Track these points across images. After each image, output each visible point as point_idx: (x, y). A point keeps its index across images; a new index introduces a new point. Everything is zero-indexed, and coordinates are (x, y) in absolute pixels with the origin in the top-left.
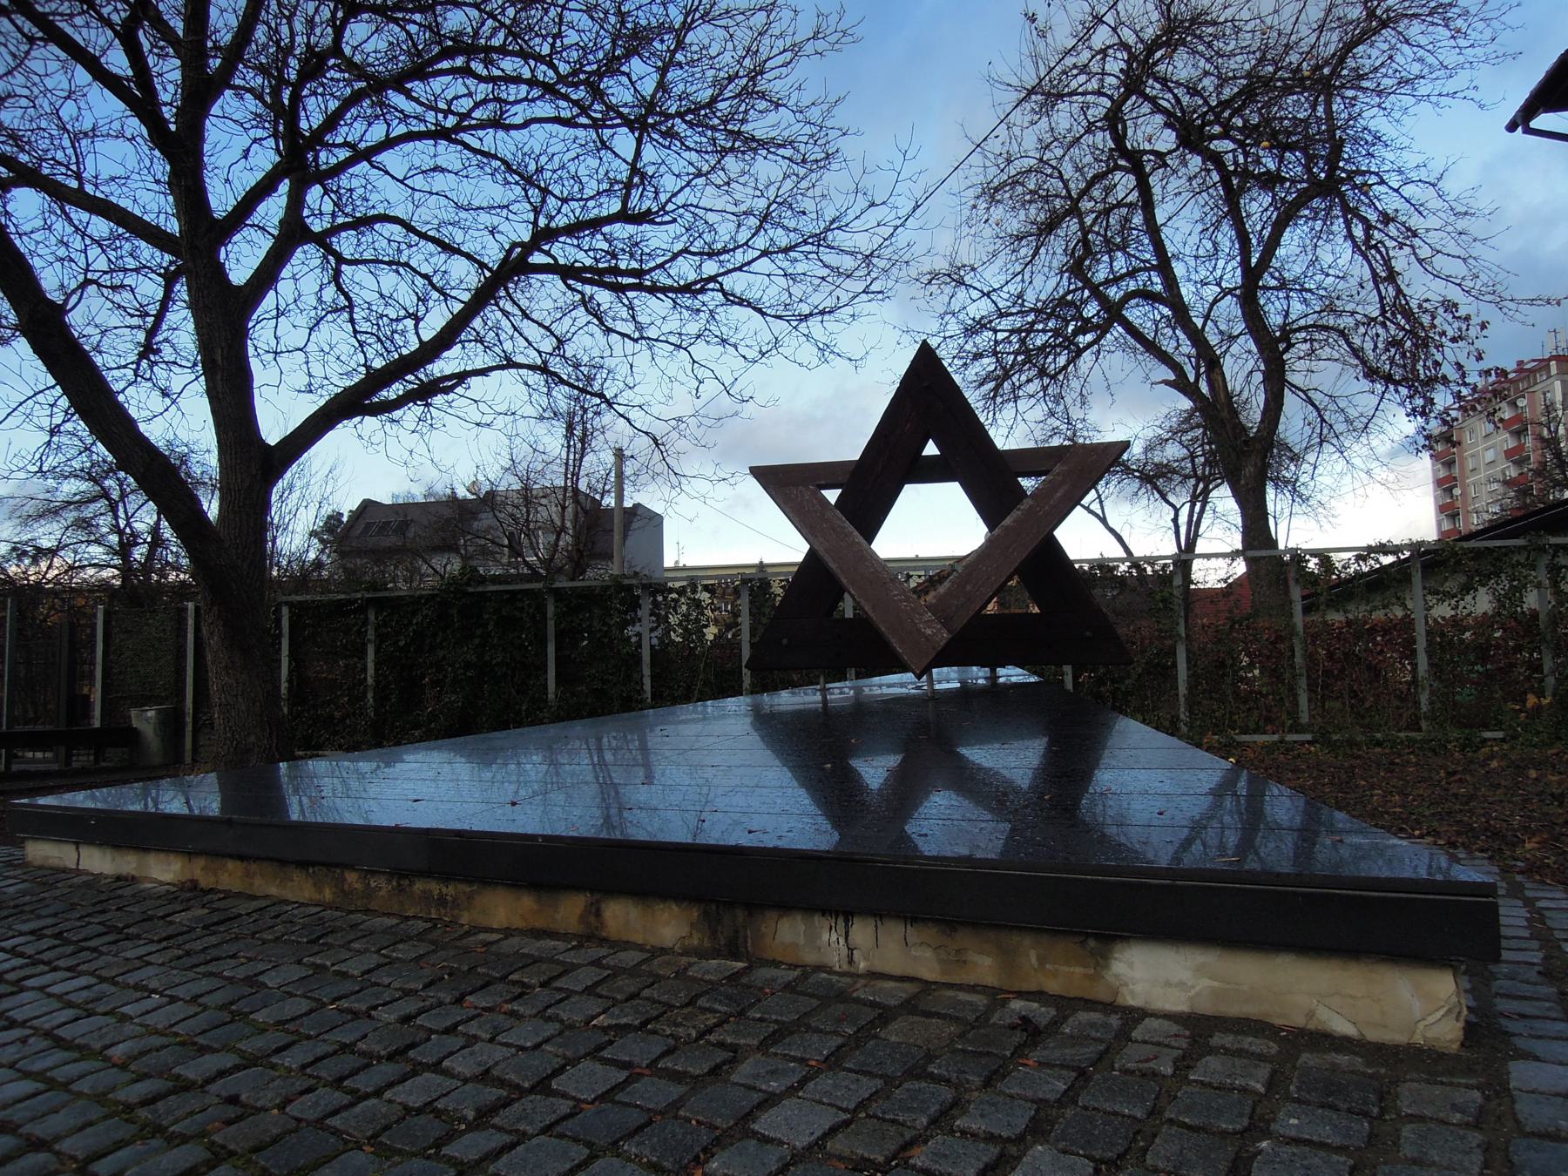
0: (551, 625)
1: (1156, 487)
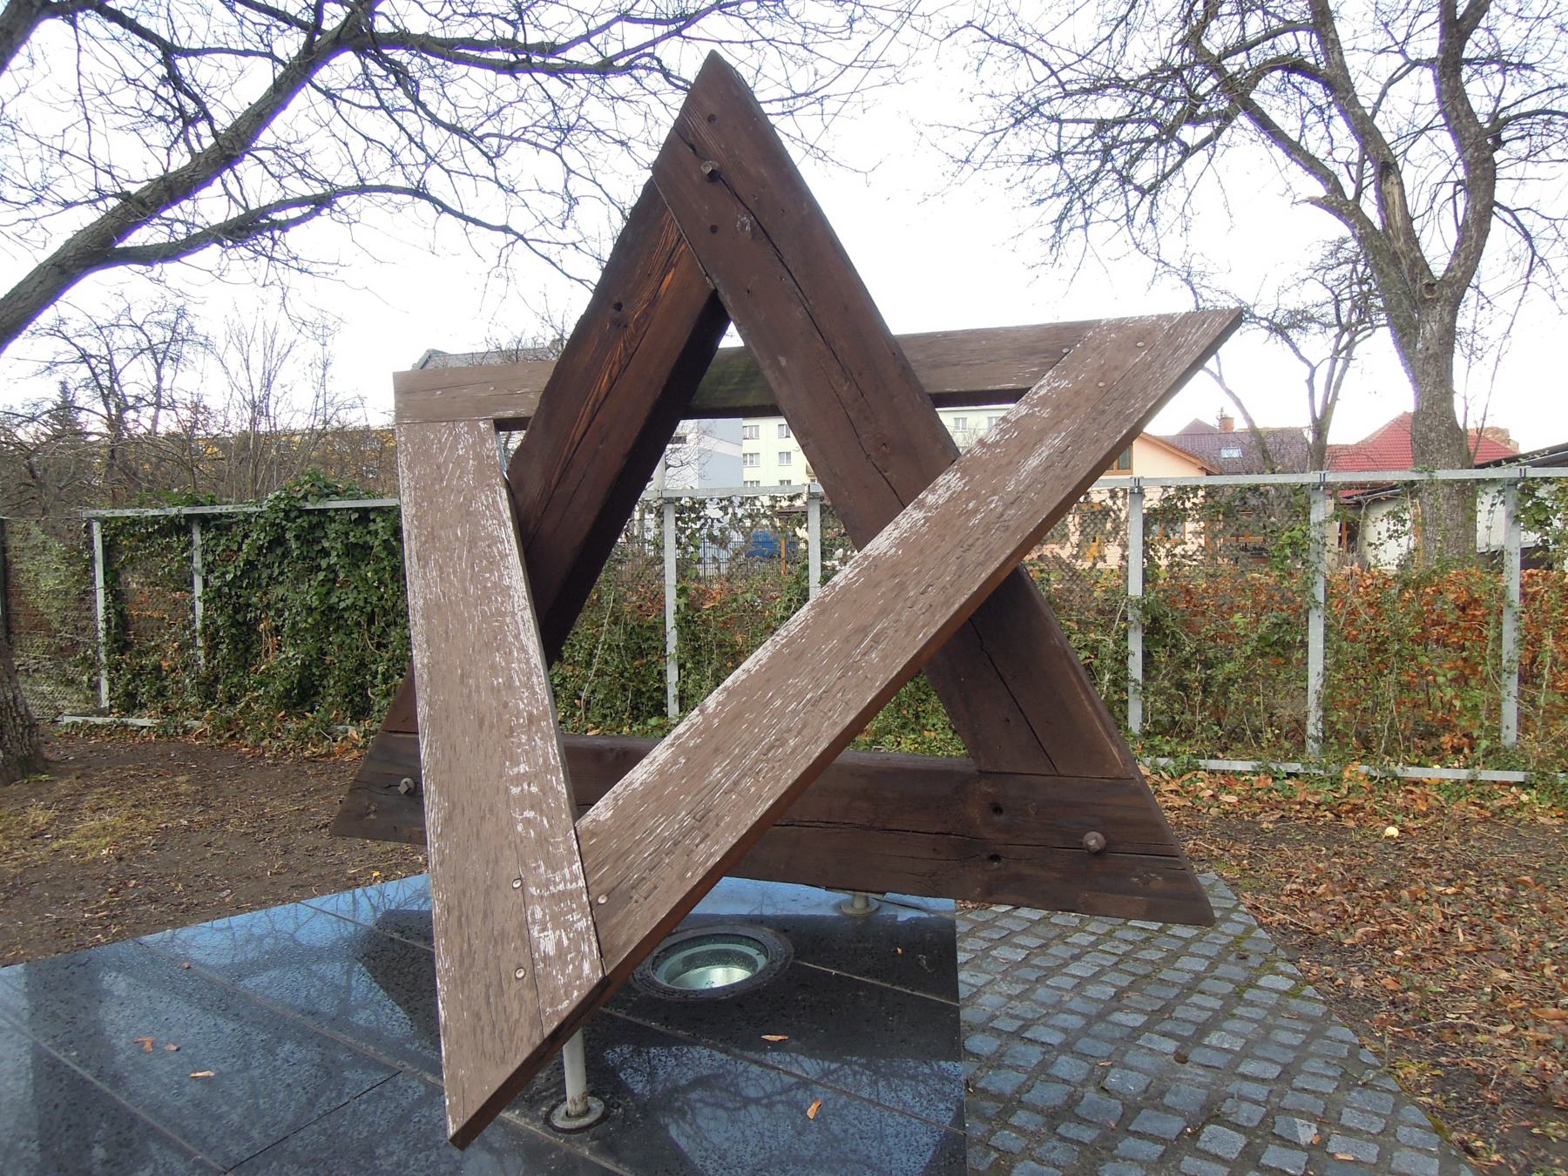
1: (1288, 339)
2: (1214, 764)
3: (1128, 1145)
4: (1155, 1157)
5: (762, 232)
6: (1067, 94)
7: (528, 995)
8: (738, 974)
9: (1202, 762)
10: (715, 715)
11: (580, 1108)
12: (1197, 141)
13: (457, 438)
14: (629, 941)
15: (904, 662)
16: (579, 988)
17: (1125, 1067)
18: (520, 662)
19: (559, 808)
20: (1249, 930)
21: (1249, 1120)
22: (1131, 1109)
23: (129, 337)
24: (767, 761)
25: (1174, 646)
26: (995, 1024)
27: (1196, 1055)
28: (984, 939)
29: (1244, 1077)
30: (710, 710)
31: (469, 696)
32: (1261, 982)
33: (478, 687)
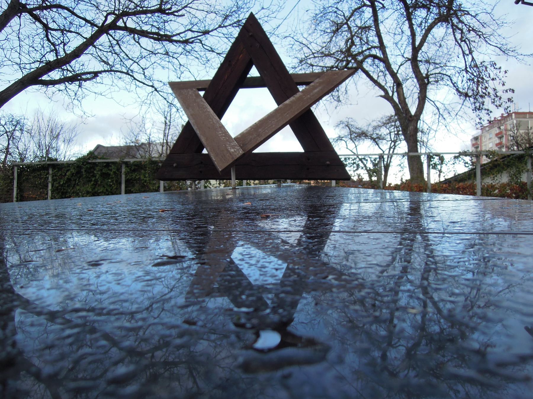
0: (123, 176)
1: (376, 142)
28: (306, 183)
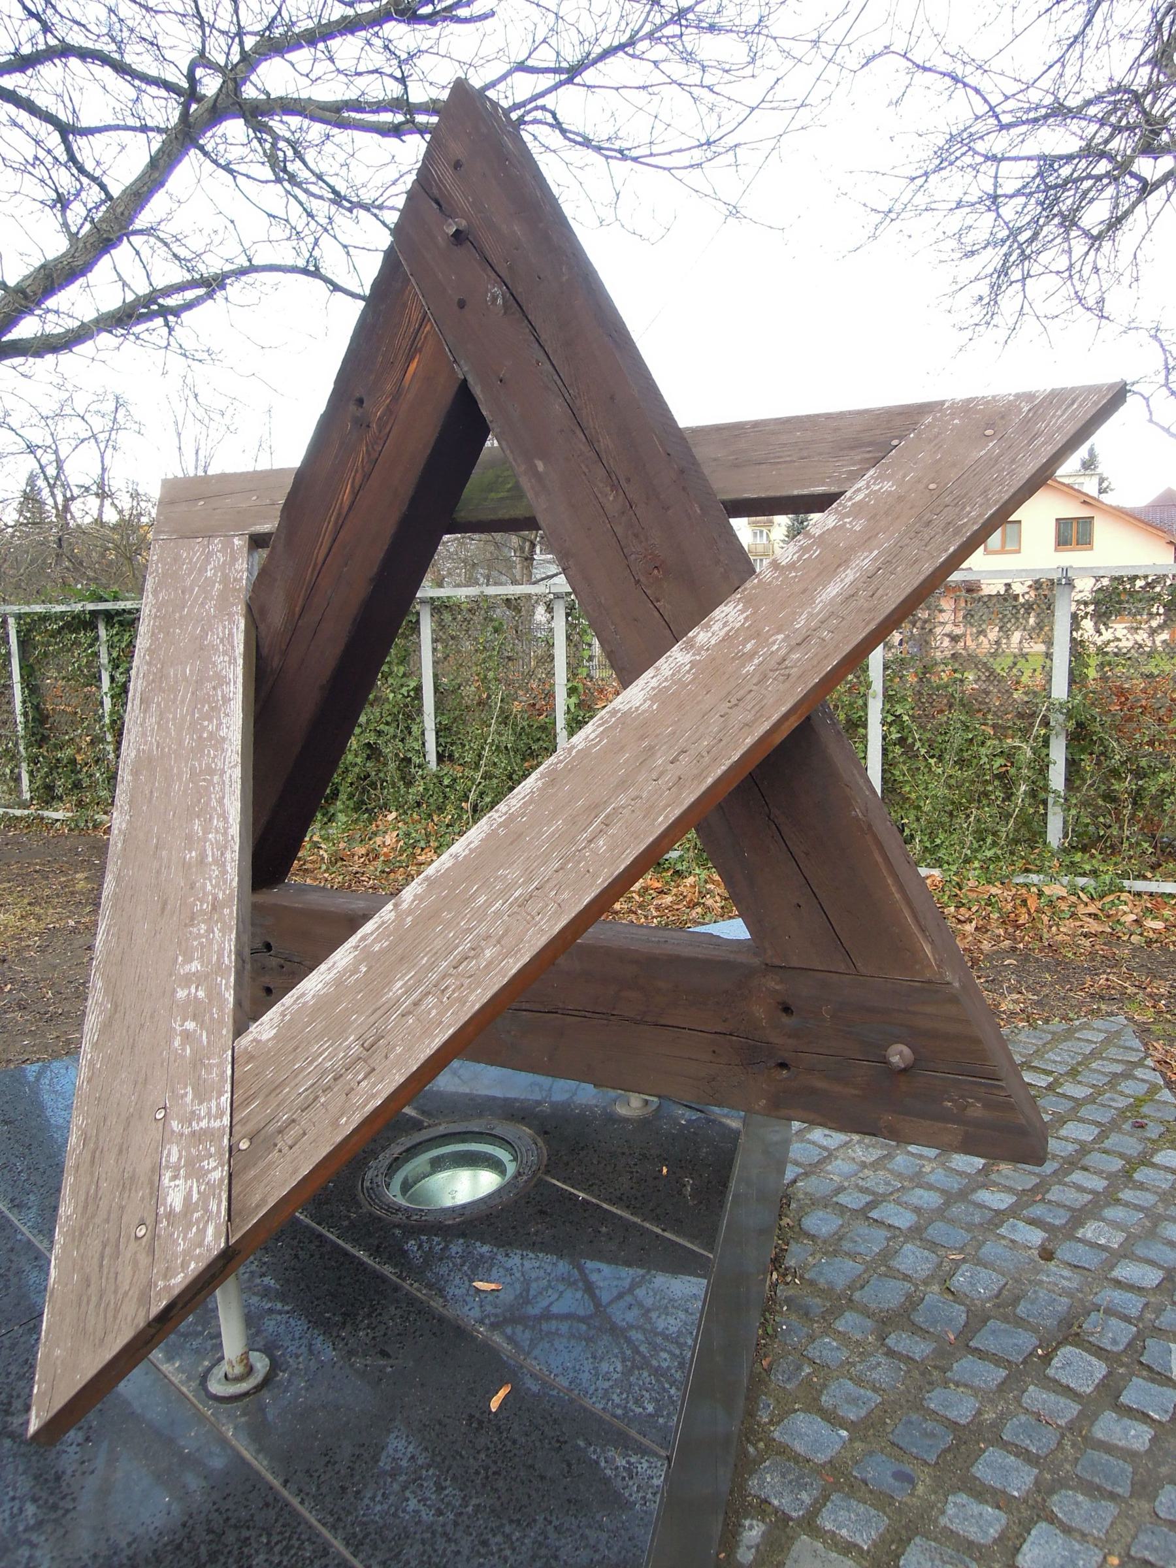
2: (1140, 885)
3: (964, 1366)
4: (993, 1385)
5: (515, 303)
6: (1003, 127)
7: (144, 1260)
8: (485, 1182)
9: (1126, 883)
10: (410, 912)
11: (238, 1370)
12: (1158, 175)
13: (210, 555)
14: (264, 1200)
15: (635, 853)
16: (198, 1258)
17: (980, 1262)
18: (217, 832)
19: (221, 1021)
20: (1154, 1089)
21: (1114, 1342)
22: (977, 1320)
23: (75, 427)
24: (457, 977)
25: (1102, 754)
26: (842, 1199)
27: (1065, 1251)
29: (1118, 1284)
30: (405, 906)
31: (158, 872)
32: (1157, 1159)
33: (170, 860)
